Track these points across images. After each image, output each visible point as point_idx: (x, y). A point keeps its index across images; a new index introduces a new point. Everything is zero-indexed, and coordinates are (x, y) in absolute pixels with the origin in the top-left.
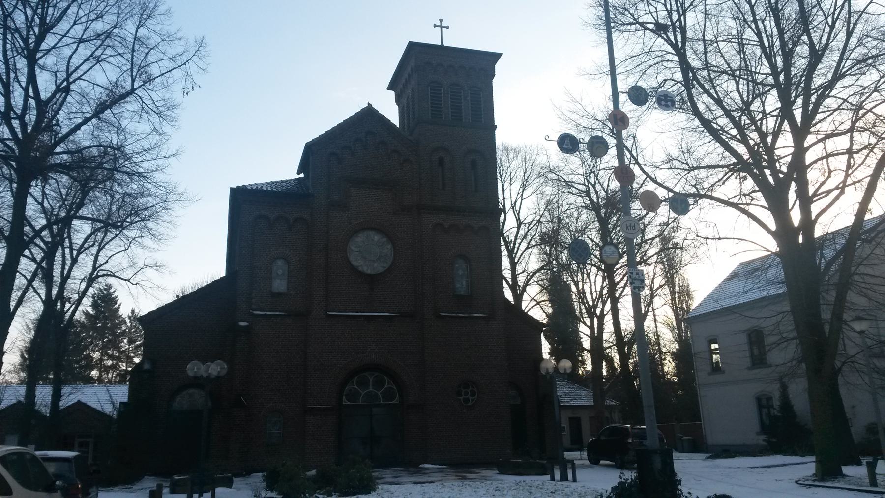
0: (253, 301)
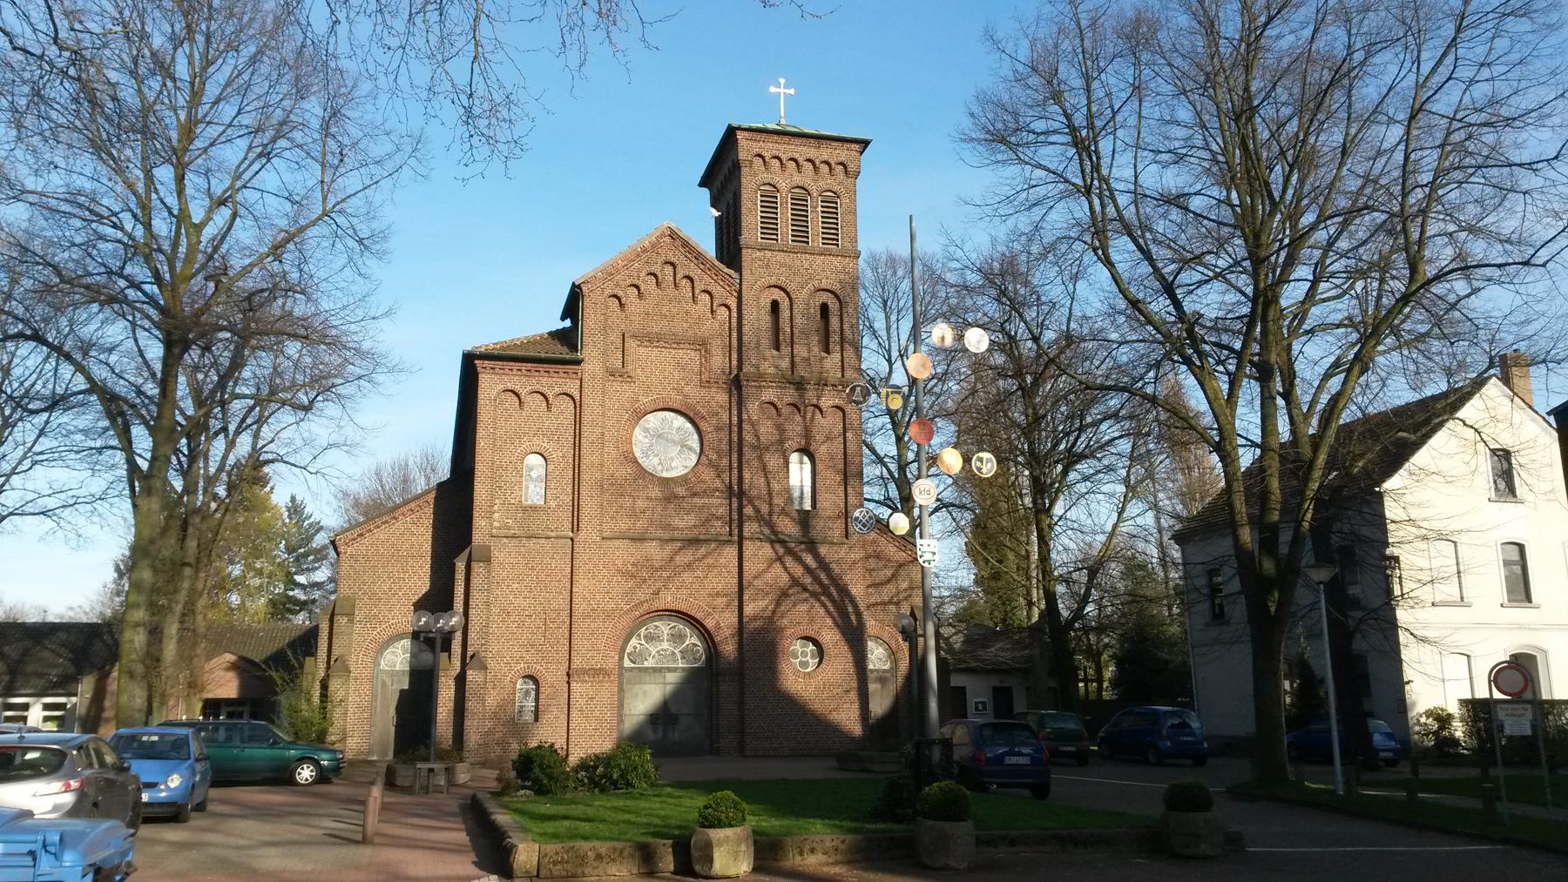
0: (496, 515)
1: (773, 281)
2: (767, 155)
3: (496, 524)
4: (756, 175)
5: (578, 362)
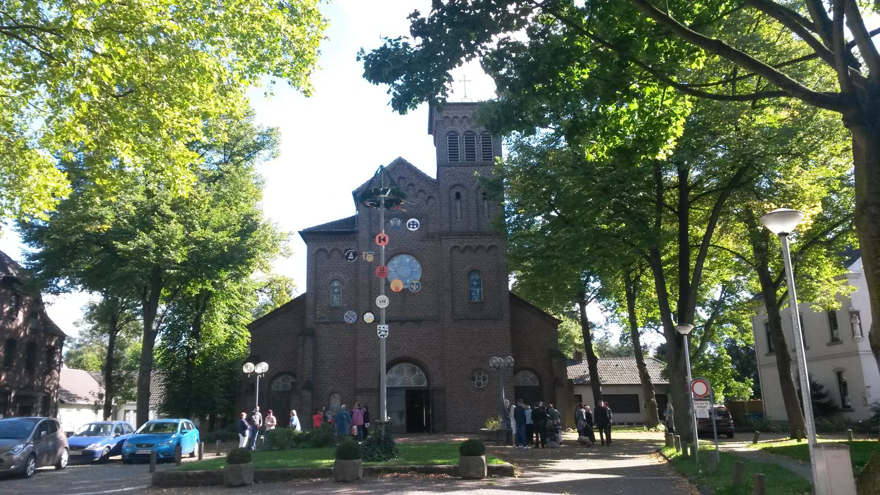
1: (456, 182)
2: (451, 116)
3: (318, 317)
4: (445, 127)
5: (356, 232)
